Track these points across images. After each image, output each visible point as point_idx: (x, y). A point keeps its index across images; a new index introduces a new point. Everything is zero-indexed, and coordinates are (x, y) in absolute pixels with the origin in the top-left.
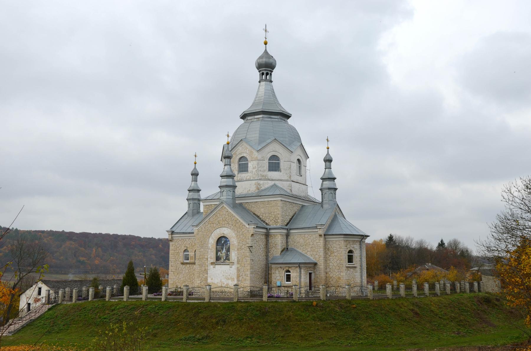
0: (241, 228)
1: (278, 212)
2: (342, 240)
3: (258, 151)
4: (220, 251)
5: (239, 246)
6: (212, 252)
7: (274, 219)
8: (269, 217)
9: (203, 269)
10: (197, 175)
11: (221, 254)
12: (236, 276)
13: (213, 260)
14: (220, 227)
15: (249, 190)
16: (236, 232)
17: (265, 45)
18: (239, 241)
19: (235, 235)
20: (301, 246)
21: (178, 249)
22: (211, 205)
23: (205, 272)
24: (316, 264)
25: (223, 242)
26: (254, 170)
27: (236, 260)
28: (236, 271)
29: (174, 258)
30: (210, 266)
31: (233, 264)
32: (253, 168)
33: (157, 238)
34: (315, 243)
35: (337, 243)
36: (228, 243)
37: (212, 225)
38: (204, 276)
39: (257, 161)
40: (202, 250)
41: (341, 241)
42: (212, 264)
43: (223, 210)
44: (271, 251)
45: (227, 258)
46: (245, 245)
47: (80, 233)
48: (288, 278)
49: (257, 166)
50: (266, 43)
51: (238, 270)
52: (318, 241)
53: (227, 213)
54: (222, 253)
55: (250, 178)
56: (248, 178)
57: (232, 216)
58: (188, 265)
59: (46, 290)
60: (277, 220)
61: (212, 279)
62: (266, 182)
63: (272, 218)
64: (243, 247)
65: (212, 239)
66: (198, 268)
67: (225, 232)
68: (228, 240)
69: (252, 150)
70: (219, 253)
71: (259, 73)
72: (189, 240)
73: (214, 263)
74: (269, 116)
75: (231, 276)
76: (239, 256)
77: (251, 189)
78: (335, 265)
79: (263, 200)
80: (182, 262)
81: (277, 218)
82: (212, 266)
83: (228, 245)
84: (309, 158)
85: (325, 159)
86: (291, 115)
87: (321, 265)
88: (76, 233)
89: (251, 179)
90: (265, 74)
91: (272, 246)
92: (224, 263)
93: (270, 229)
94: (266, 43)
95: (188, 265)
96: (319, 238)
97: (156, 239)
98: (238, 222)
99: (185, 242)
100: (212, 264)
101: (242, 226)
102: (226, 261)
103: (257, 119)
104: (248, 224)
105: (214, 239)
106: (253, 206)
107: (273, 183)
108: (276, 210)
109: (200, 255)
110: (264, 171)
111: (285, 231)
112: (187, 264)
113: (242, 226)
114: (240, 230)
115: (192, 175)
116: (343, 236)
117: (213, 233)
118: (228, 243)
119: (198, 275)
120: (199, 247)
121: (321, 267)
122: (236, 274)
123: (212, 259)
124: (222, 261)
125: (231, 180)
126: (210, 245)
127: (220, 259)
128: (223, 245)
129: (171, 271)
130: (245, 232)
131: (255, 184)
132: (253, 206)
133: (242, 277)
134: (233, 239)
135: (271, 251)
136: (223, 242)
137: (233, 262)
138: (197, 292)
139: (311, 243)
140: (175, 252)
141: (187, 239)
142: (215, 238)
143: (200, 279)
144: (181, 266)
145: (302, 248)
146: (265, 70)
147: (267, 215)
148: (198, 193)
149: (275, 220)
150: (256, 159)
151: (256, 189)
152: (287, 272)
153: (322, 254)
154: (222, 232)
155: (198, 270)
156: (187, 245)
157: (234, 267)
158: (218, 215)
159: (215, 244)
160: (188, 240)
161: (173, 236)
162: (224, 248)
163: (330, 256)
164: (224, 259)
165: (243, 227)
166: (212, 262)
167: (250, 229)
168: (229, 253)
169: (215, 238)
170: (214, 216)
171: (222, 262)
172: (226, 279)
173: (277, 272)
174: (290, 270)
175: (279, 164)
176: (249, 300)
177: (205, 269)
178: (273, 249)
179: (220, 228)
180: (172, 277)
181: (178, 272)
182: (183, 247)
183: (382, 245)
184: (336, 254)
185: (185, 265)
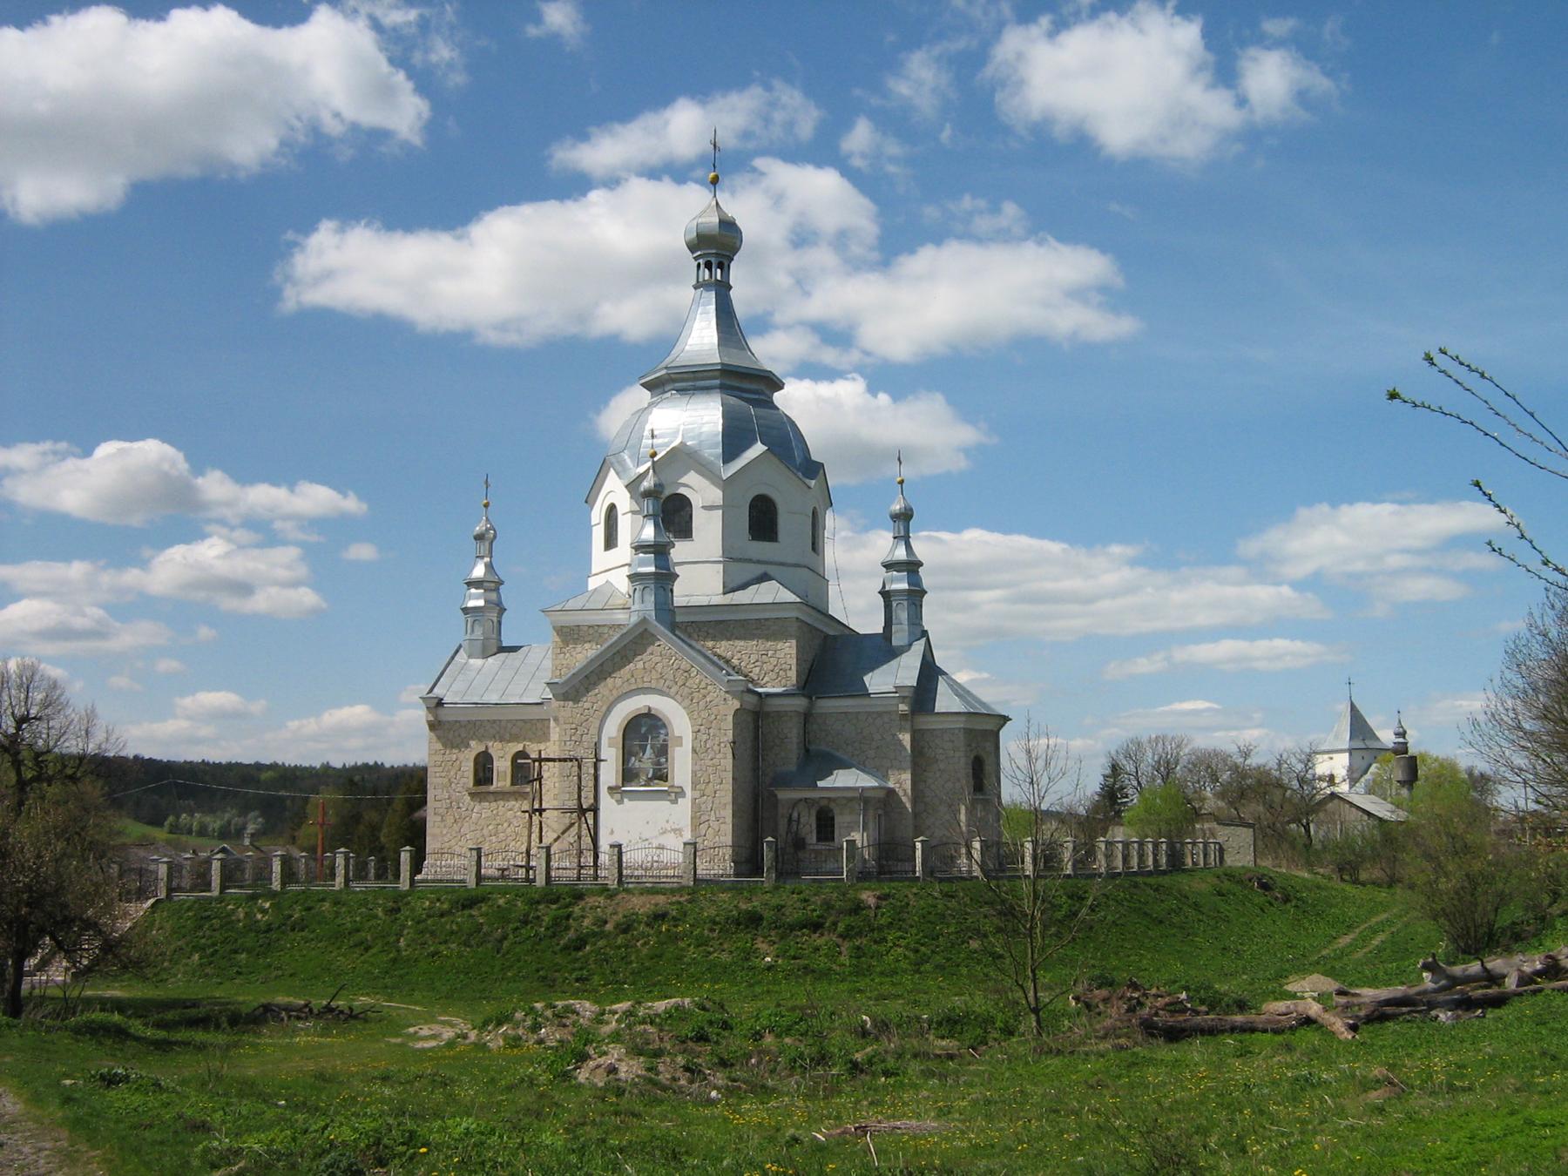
18: (696, 729)
25: (643, 730)
33: (318, 767)
45: (661, 776)
47: (544, 199)
63: (771, 667)
68: (660, 723)
74: (738, 385)
76: (698, 768)
83: (662, 737)
88: (324, 485)
97: (314, 768)
136: (643, 730)
157: (685, 804)
162: (649, 747)
164: (650, 776)
168: (663, 760)
180: (437, 831)
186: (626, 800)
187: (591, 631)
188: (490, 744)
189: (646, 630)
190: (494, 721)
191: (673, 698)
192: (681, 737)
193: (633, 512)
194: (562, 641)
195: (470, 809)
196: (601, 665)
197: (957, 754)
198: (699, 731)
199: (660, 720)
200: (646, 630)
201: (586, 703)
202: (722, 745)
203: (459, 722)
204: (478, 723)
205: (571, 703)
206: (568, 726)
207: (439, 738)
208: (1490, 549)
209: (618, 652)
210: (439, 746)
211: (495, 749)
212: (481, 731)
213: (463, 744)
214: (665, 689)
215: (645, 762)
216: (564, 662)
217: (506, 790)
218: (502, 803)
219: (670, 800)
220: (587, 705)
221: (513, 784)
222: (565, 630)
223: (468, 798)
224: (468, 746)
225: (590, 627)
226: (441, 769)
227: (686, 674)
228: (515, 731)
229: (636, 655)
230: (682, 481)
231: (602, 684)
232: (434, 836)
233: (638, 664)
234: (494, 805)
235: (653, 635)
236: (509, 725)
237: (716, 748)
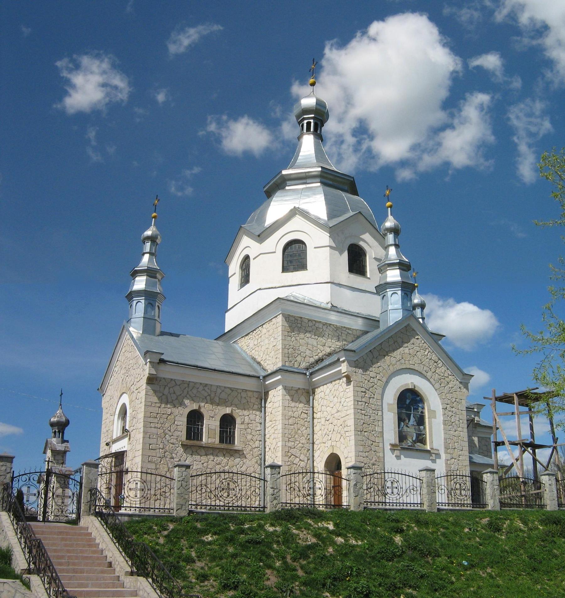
3: (259, 236)
25: (408, 401)
36: (420, 405)
45: (421, 439)
54: (409, 425)
59: (374, 40)
68: (418, 398)
76: (447, 436)
83: (420, 409)
102: (419, 444)
118: (420, 405)
124: (410, 444)
138: (461, 489)
164: (414, 439)
168: (422, 427)
183: (270, 532)
186: (402, 456)
187: (310, 324)
188: (202, 404)
189: (408, 325)
190: (206, 385)
191: (429, 380)
192: (435, 411)
193: (331, 247)
194: (290, 327)
196: (381, 344)
198: (446, 409)
200: (408, 325)
201: (373, 370)
202: (461, 421)
203: (175, 380)
204: (191, 384)
205: (361, 370)
207: (155, 391)
209: (391, 337)
210: (155, 399)
211: (207, 409)
212: (195, 391)
213: (178, 402)
214: (424, 372)
216: (291, 344)
217: (215, 446)
218: (212, 457)
219: (431, 460)
220: (372, 374)
221: (221, 441)
222: (291, 318)
223: (181, 450)
224: (182, 404)
225: (309, 320)
226: (156, 420)
227: (435, 364)
228: (223, 396)
229: (403, 343)
230: (362, 237)
231: (383, 360)
233: (404, 350)
234: (204, 458)
235: (413, 330)
236: (219, 391)
237: (457, 422)
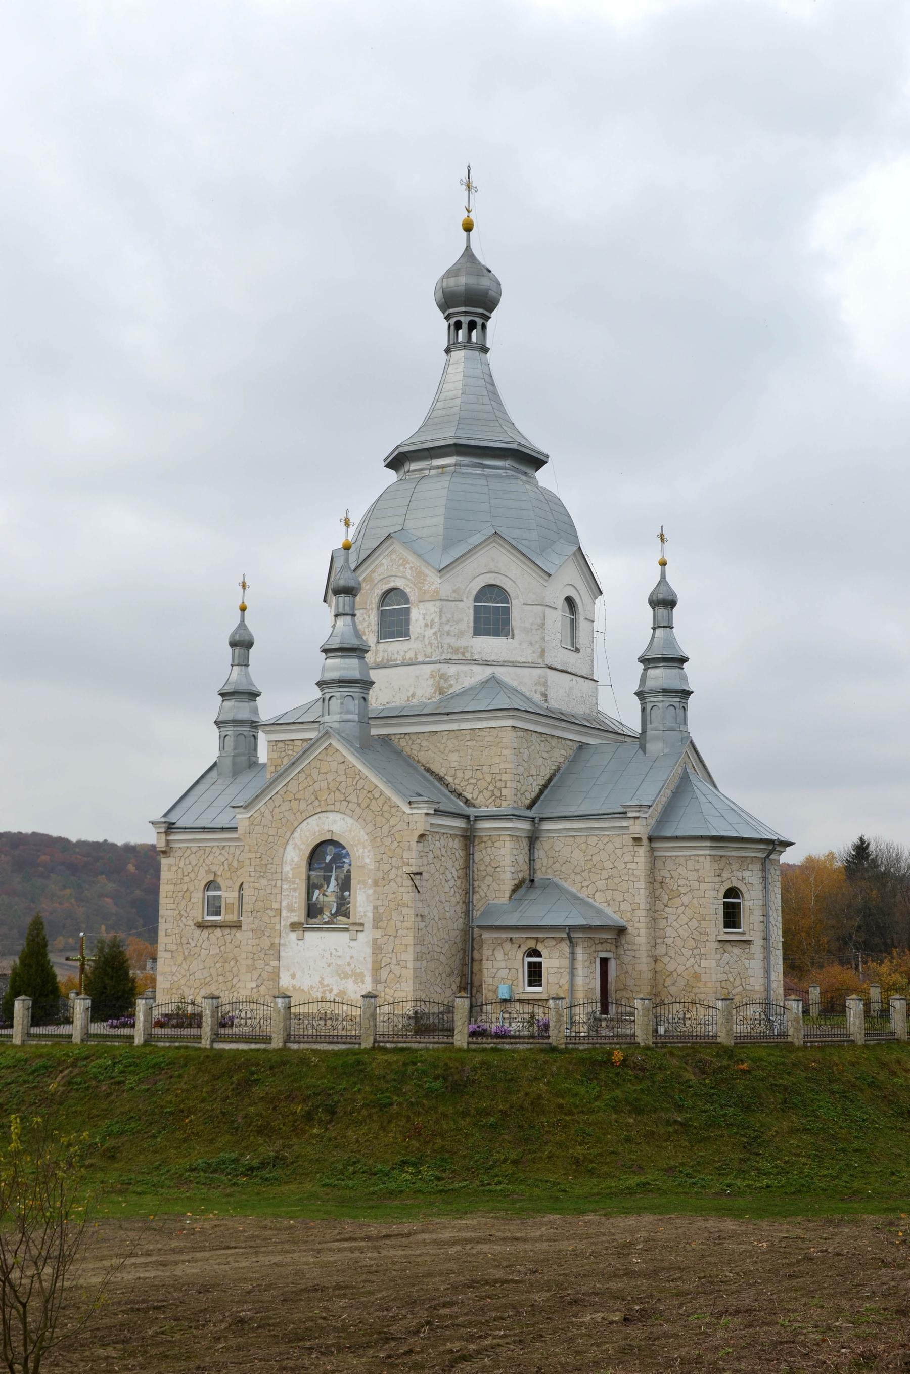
0: (387, 815)
1: (502, 766)
2: (705, 855)
4: (319, 887)
5: (379, 870)
6: (295, 890)
7: (491, 788)
8: (475, 781)
9: (266, 943)
10: (249, 645)
11: (321, 898)
12: (370, 966)
13: (299, 915)
14: (318, 810)
15: (413, 695)
16: (370, 827)
17: (465, 233)
18: (379, 857)
19: (366, 837)
20: (576, 874)
21: (186, 879)
22: (293, 740)
23: (272, 952)
24: (621, 931)
25: (328, 858)
26: (429, 632)
27: (370, 915)
28: (368, 951)
29: (174, 906)
30: (287, 934)
31: (360, 928)
32: (426, 625)
34: (621, 866)
35: (691, 864)
37: (295, 804)
38: (269, 965)
39: (438, 603)
40: (264, 882)
41: (702, 859)
42: (294, 926)
43: (329, 759)
44: (479, 887)
45: (343, 909)
46: (398, 868)
48: (535, 975)
49: (437, 619)
50: (468, 227)
51: (377, 948)
52: (628, 858)
53: (343, 767)
55: (416, 655)
56: (410, 655)
57: (358, 777)
58: (219, 930)
60: (500, 789)
61: (293, 976)
62: (466, 668)
63: (486, 785)
64: (392, 876)
65: (294, 848)
66: (250, 942)
67: (335, 828)
68: (344, 851)
69: (423, 568)
70: (317, 892)
71: (445, 324)
72: (223, 851)
73: (301, 924)
75: (353, 966)
76: (379, 903)
77: (419, 693)
78: (684, 932)
79: (454, 726)
80: (200, 920)
81: (499, 784)
82: (293, 936)
83: (346, 867)
84: (601, 593)
85: (654, 598)
86: (547, 456)
87: (638, 935)
89: (420, 659)
90: (465, 326)
91: (484, 874)
92: (330, 927)
93: (478, 818)
94: (468, 227)
95: (218, 932)
96: (631, 848)
98: (376, 796)
99: (211, 857)
100: (294, 926)
101: (391, 807)
102: (339, 918)
103: (440, 470)
104: (410, 803)
105: (300, 850)
106: (425, 744)
107: (488, 671)
108: (497, 759)
109: (256, 900)
110: (461, 634)
111: (525, 826)
112: (215, 926)
113: (391, 807)
114: (384, 820)
115: (233, 644)
116: (708, 844)
117: (298, 830)
119: (250, 962)
120: (252, 874)
121: (638, 940)
122: (370, 960)
123: (293, 911)
125: (355, 662)
126: (287, 868)
127: (320, 911)
128: (328, 868)
129: (165, 950)
130: (398, 828)
131: (432, 676)
132: (425, 744)
133: (388, 969)
134: (361, 851)
135: (479, 887)
136: (328, 858)
137: (361, 921)
139: (608, 865)
140: (178, 888)
141: (213, 850)
142: (303, 847)
143: (256, 974)
144: (198, 932)
145: (578, 878)
146: (465, 312)
147: (468, 774)
148: (252, 703)
149: (493, 791)
150: (436, 597)
151: (435, 693)
152: (529, 955)
153: (641, 898)
154: (326, 828)
155: (250, 948)
156: (214, 868)
158: (315, 773)
159: (304, 864)
160: (218, 852)
161: (171, 838)
163: (666, 906)
164: (334, 911)
165: (394, 810)
166: (292, 920)
167: (416, 818)
168: (347, 893)
169: (303, 847)
170: (302, 776)
171: (326, 923)
172: (339, 975)
173: (499, 955)
174: (540, 947)
175: (506, 611)
176: (409, 1045)
177: (272, 944)
178: (488, 880)
179: (320, 815)
181: (186, 954)
182: (202, 872)
184: (685, 900)
185: (210, 930)
195: (199, 945)
197: (703, 886)
199: (344, 848)
206: (253, 855)
208: (247, 591)
215: (328, 895)
232: (163, 974)
